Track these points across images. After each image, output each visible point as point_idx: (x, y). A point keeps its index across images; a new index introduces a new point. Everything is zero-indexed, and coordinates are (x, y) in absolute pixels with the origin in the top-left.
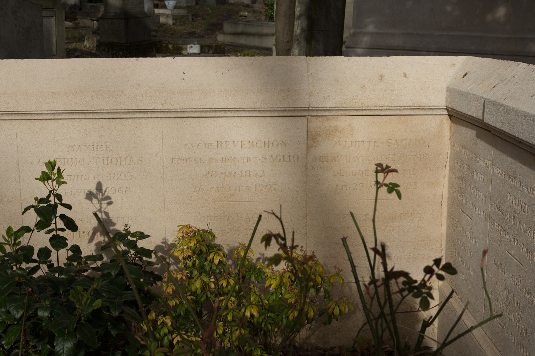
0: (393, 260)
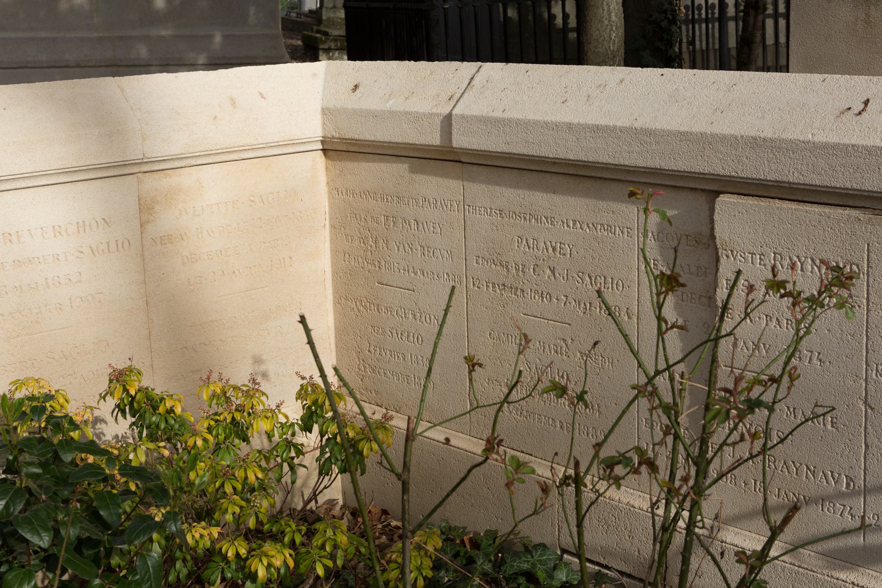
0: (273, 380)
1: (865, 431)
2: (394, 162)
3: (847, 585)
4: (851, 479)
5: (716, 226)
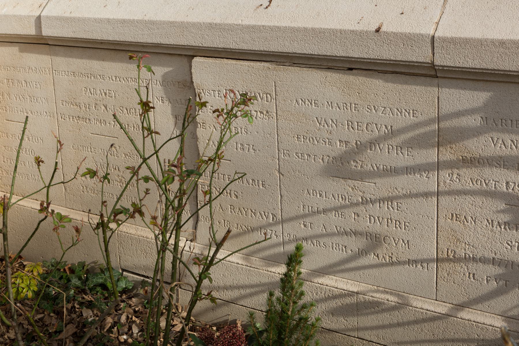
1: (280, 188)
2: (9, 46)
3: (276, 275)
4: (275, 216)
5: (193, 76)
